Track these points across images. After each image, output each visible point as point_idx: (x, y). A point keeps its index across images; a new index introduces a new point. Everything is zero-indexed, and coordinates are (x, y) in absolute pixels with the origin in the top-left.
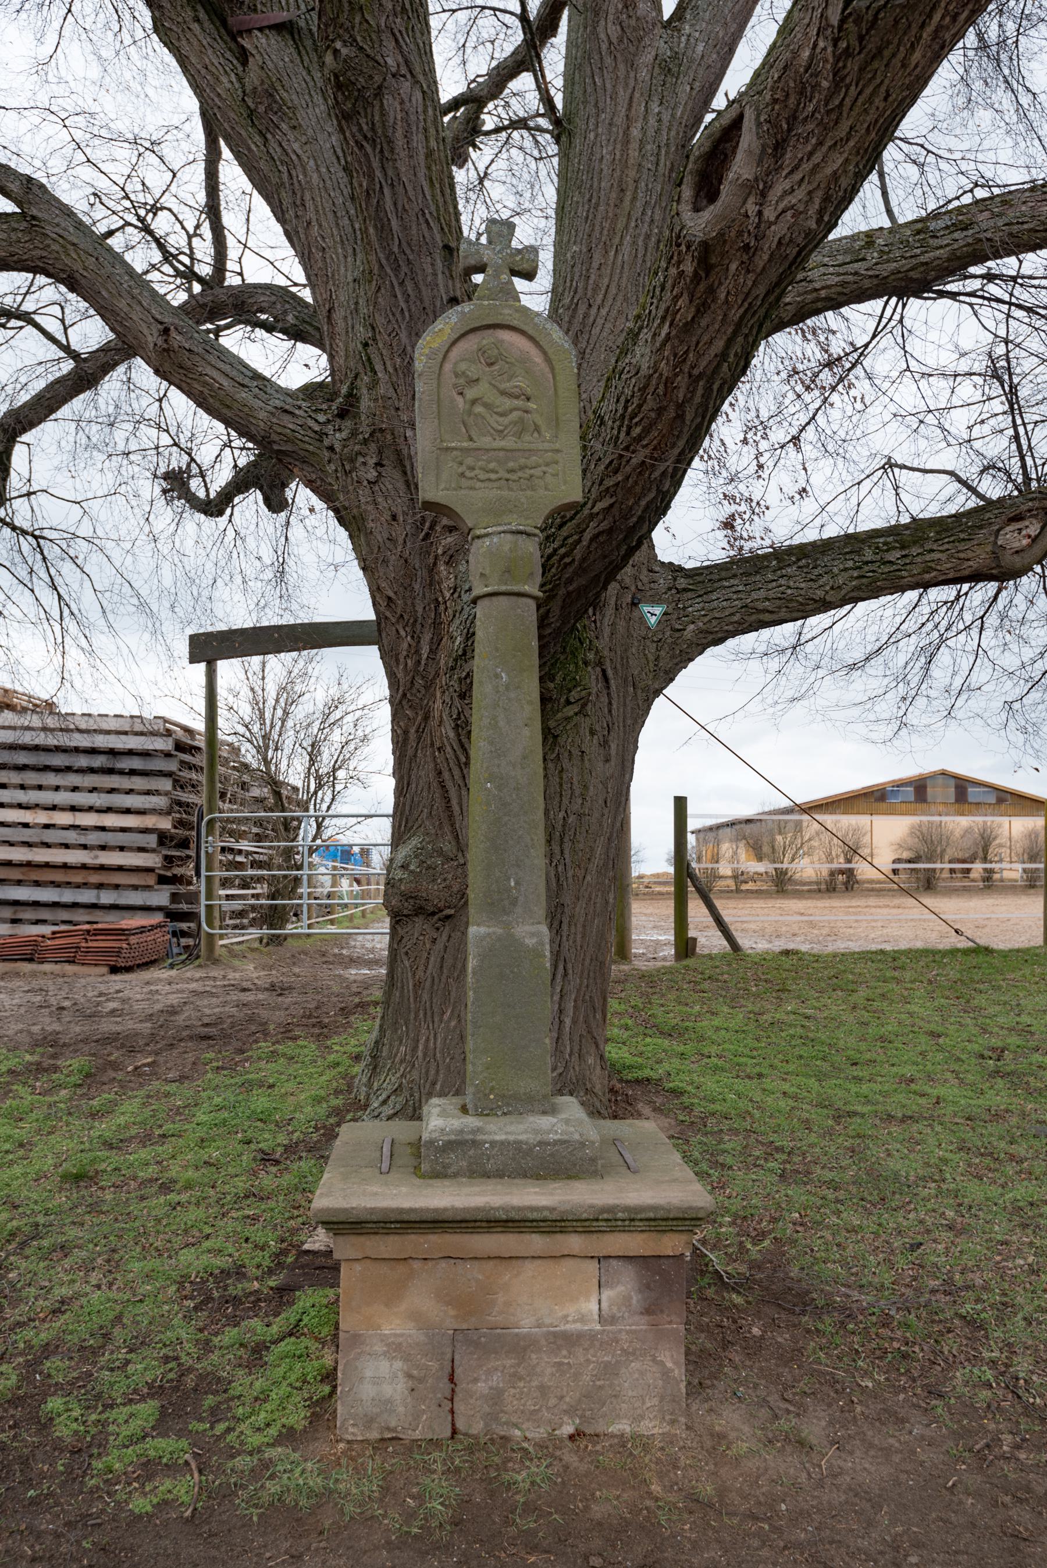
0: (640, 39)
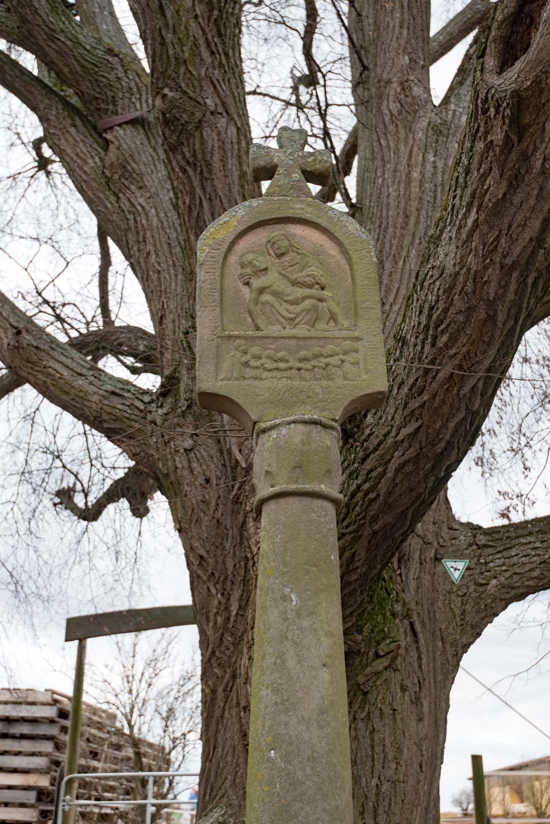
0: (416, 112)
